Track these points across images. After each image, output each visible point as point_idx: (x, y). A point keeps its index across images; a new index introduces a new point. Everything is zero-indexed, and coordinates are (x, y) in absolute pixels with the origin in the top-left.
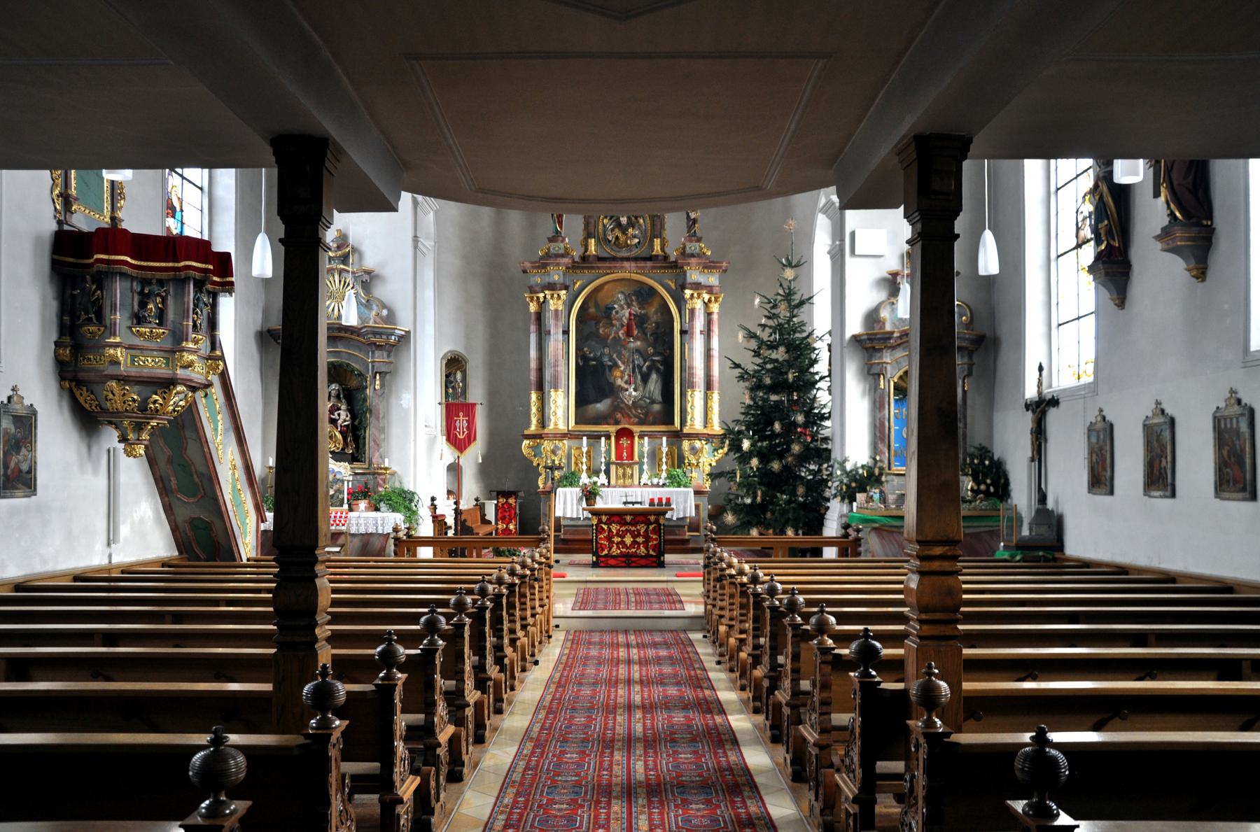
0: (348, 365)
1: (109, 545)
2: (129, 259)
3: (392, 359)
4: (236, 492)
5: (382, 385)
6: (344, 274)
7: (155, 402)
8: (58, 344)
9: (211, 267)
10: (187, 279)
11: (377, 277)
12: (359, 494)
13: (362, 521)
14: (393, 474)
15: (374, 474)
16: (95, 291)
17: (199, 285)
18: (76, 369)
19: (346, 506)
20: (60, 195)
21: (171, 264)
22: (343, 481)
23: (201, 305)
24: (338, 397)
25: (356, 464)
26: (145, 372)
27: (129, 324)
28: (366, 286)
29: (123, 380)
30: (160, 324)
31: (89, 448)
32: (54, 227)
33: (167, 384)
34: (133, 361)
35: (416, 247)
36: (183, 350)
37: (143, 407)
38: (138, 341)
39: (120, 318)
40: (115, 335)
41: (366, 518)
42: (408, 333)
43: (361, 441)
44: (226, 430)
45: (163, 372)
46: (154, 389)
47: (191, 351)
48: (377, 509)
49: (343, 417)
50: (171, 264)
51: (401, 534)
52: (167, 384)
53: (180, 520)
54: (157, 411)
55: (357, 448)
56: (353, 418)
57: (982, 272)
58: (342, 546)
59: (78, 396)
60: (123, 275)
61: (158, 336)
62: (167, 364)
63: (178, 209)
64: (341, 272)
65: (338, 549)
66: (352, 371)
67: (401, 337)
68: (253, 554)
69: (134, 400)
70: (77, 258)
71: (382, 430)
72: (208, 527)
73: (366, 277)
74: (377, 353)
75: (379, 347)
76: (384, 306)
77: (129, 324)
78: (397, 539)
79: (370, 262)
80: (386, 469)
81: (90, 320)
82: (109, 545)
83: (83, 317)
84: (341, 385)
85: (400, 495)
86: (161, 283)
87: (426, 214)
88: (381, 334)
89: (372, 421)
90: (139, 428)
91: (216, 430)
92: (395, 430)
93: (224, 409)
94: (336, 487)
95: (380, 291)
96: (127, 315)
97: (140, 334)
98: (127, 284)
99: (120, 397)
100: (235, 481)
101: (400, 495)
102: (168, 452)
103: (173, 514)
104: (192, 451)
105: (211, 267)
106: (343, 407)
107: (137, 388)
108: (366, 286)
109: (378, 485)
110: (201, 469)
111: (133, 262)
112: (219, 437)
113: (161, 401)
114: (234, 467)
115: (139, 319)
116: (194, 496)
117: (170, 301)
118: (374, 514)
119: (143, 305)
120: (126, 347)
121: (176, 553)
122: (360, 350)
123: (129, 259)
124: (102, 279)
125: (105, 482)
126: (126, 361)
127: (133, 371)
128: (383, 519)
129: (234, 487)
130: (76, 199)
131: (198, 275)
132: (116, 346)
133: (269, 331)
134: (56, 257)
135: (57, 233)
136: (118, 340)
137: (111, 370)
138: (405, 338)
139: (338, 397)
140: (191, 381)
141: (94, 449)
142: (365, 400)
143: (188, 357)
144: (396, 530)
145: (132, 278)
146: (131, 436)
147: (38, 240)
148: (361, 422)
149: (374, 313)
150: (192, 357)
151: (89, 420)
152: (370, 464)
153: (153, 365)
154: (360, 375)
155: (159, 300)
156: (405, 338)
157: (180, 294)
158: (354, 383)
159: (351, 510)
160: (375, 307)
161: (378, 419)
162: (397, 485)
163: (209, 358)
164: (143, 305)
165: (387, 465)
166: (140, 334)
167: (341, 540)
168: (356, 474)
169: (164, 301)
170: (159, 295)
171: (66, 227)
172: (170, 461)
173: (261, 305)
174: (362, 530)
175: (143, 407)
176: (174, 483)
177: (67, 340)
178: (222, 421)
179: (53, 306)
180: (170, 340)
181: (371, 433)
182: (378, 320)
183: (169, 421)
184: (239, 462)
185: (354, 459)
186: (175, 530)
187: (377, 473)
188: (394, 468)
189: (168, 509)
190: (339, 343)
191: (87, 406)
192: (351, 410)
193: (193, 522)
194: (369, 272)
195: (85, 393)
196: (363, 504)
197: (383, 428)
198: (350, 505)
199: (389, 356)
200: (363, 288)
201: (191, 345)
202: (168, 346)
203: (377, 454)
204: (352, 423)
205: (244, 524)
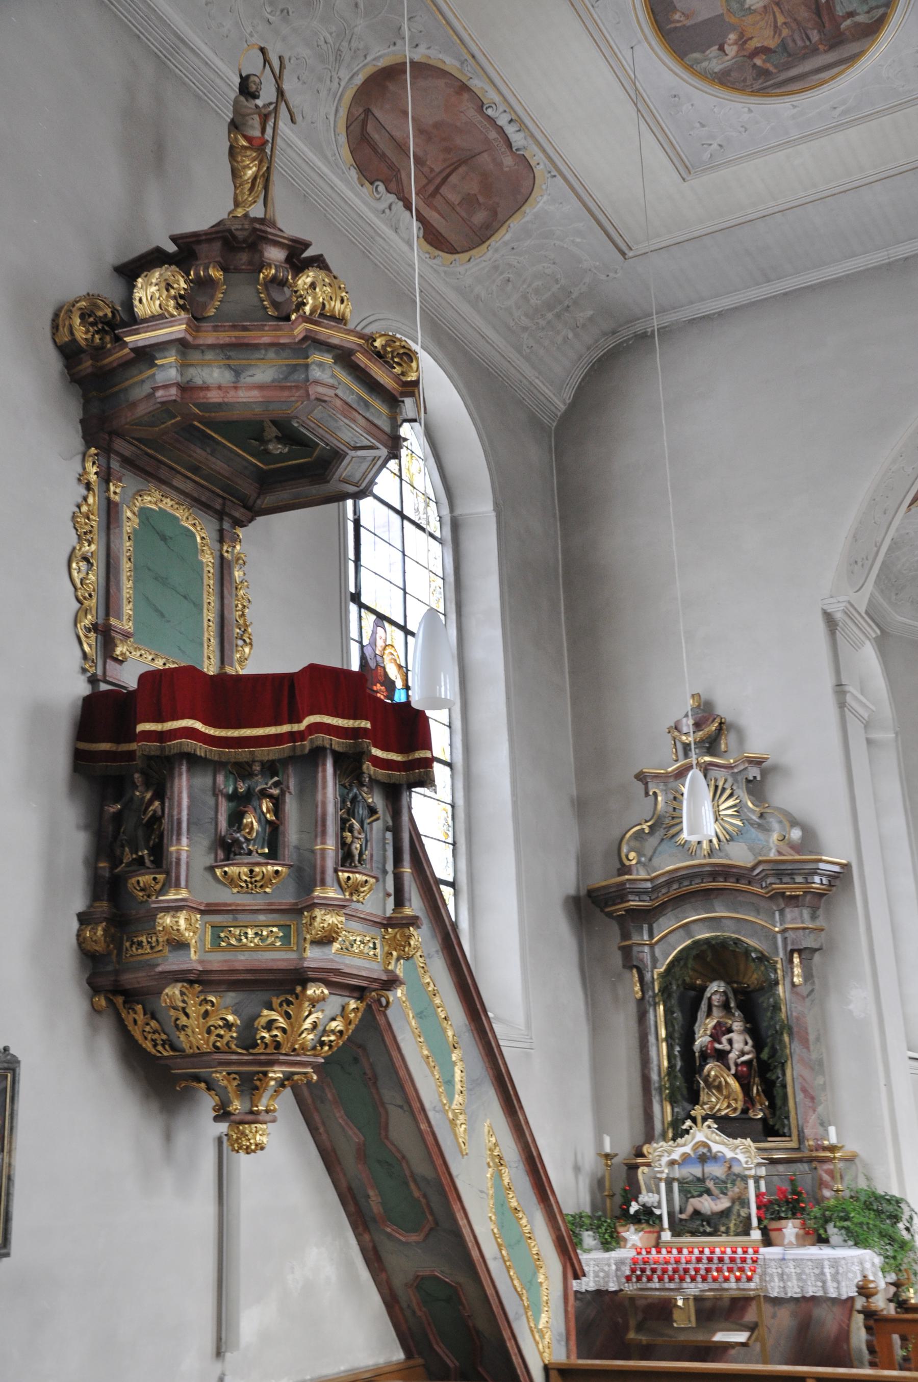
0: (737, 942)
1: (219, 1353)
2: (198, 725)
3: (820, 922)
4: (506, 1215)
5: (808, 976)
6: (714, 773)
7: (270, 1025)
8: (84, 919)
9: (367, 724)
10: (317, 754)
11: (775, 769)
12: (784, 1205)
13: (791, 1269)
14: (851, 1159)
15: (811, 1160)
16: (151, 802)
17: (350, 766)
18: (114, 968)
19: (756, 1235)
20: (95, 627)
21: (285, 728)
22: (744, 1179)
23: (361, 811)
24: (726, 1006)
25: (773, 1142)
26: (242, 960)
27: (209, 860)
28: (755, 788)
29: (202, 980)
30: (273, 855)
31: (168, 1136)
32: (83, 689)
33: (289, 983)
34: (217, 939)
35: (842, 705)
36: (312, 906)
37: (248, 1041)
38: (226, 896)
39: (187, 849)
40: (177, 885)
41: (798, 1262)
42: (846, 867)
43: (778, 1091)
44: (472, 1086)
45: (279, 958)
46: (262, 996)
47: (328, 906)
48: (823, 1240)
49: (738, 1045)
50: (285, 728)
51: (881, 1303)
52: (289, 983)
53: (398, 1282)
54: (278, 1045)
55: (772, 1106)
56: (758, 1046)
57: (798, 1222)
58: (752, 1328)
59: (129, 1023)
60: (193, 760)
61: (266, 880)
62: (286, 939)
63: (399, 684)
64: (706, 769)
65: (741, 1337)
66: (747, 951)
67: (834, 878)
68: (559, 1355)
69: (228, 1026)
70: (118, 741)
71: (818, 1067)
72: (452, 1295)
73: (753, 772)
74: (790, 913)
75: (793, 900)
76: (794, 823)
77: (209, 860)
78: (870, 1315)
79: (756, 746)
80: (832, 1148)
81: (140, 861)
82: (219, 1353)
83: (128, 857)
84: (728, 983)
85: (868, 1206)
86: (271, 768)
87: (857, 647)
88: (792, 874)
89: (794, 1048)
90: (251, 1085)
91: (449, 1082)
92: (845, 1068)
93: (468, 1039)
94: (735, 1191)
95: (785, 795)
96: (204, 842)
97: (231, 881)
98: (204, 781)
99: (202, 1022)
100: (502, 1191)
101: (868, 1206)
102: (356, 1137)
103: (383, 1269)
104: (400, 1130)
105: (367, 724)
106: (737, 1026)
107: (231, 997)
108: (755, 788)
109: (822, 1184)
110: (428, 1173)
111: (211, 731)
112: (458, 1098)
113: (282, 1022)
114: (500, 1161)
115: (228, 848)
116: (414, 1230)
117: (291, 805)
118: (815, 1251)
119: (236, 819)
120: (195, 917)
121: (400, 1355)
122: (758, 911)
123: (198, 725)
124: (160, 770)
125: (210, 1209)
126: (202, 940)
127: (217, 961)
128: (835, 1263)
129: (501, 1205)
130: (127, 636)
131: (337, 743)
132: (175, 908)
133: (590, 893)
134: (84, 746)
135: (89, 703)
136: (184, 894)
137: (172, 962)
138: (841, 878)
139: (726, 1006)
140: (337, 972)
141: (182, 1138)
142: (776, 1008)
143: (326, 919)
144: (864, 1290)
145: (217, 766)
146: (237, 1106)
147: (39, 714)
148: (774, 1053)
149: (775, 836)
150: (332, 919)
151: (162, 1076)
152: (801, 1139)
153: (259, 945)
154: (762, 958)
155: (265, 805)
156: (841, 878)
157: (309, 788)
158: (753, 978)
159: (768, 1242)
160: (776, 826)
161: (805, 1043)
162: (862, 1184)
163: (387, 923)
164: (236, 819)
165: (833, 1138)
166: (231, 881)
167: (750, 1316)
168: (773, 1162)
169: (278, 804)
170: (264, 794)
171: (104, 687)
172: (362, 1154)
173: (572, 848)
174: (794, 1291)
175: (248, 1041)
176: (375, 1203)
177: (104, 906)
178: (464, 1063)
179: (76, 844)
180: (291, 887)
181: (794, 1074)
182: (786, 849)
183: (317, 1068)
184: (510, 1150)
185: (770, 1129)
186: (391, 1302)
187: (817, 1157)
188: (851, 1146)
189: (374, 1260)
190: (717, 904)
191: (148, 1046)
192: (753, 1031)
193: (421, 1283)
194: (757, 762)
195: (140, 1018)
196: (790, 1229)
197: (820, 1063)
198: (765, 1231)
199: (814, 917)
200: (750, 792)
201: (332, 893)
202: (288, 899)
203: (813, 1118)
204: (758, 1057)
205: (532, 1285)
